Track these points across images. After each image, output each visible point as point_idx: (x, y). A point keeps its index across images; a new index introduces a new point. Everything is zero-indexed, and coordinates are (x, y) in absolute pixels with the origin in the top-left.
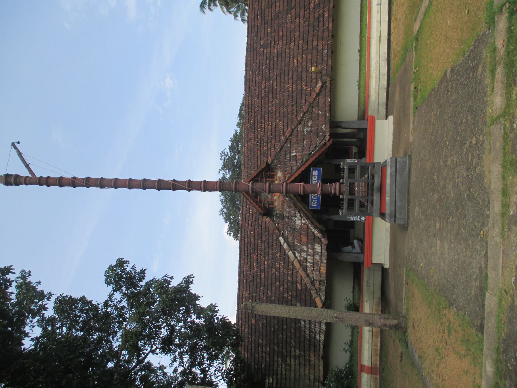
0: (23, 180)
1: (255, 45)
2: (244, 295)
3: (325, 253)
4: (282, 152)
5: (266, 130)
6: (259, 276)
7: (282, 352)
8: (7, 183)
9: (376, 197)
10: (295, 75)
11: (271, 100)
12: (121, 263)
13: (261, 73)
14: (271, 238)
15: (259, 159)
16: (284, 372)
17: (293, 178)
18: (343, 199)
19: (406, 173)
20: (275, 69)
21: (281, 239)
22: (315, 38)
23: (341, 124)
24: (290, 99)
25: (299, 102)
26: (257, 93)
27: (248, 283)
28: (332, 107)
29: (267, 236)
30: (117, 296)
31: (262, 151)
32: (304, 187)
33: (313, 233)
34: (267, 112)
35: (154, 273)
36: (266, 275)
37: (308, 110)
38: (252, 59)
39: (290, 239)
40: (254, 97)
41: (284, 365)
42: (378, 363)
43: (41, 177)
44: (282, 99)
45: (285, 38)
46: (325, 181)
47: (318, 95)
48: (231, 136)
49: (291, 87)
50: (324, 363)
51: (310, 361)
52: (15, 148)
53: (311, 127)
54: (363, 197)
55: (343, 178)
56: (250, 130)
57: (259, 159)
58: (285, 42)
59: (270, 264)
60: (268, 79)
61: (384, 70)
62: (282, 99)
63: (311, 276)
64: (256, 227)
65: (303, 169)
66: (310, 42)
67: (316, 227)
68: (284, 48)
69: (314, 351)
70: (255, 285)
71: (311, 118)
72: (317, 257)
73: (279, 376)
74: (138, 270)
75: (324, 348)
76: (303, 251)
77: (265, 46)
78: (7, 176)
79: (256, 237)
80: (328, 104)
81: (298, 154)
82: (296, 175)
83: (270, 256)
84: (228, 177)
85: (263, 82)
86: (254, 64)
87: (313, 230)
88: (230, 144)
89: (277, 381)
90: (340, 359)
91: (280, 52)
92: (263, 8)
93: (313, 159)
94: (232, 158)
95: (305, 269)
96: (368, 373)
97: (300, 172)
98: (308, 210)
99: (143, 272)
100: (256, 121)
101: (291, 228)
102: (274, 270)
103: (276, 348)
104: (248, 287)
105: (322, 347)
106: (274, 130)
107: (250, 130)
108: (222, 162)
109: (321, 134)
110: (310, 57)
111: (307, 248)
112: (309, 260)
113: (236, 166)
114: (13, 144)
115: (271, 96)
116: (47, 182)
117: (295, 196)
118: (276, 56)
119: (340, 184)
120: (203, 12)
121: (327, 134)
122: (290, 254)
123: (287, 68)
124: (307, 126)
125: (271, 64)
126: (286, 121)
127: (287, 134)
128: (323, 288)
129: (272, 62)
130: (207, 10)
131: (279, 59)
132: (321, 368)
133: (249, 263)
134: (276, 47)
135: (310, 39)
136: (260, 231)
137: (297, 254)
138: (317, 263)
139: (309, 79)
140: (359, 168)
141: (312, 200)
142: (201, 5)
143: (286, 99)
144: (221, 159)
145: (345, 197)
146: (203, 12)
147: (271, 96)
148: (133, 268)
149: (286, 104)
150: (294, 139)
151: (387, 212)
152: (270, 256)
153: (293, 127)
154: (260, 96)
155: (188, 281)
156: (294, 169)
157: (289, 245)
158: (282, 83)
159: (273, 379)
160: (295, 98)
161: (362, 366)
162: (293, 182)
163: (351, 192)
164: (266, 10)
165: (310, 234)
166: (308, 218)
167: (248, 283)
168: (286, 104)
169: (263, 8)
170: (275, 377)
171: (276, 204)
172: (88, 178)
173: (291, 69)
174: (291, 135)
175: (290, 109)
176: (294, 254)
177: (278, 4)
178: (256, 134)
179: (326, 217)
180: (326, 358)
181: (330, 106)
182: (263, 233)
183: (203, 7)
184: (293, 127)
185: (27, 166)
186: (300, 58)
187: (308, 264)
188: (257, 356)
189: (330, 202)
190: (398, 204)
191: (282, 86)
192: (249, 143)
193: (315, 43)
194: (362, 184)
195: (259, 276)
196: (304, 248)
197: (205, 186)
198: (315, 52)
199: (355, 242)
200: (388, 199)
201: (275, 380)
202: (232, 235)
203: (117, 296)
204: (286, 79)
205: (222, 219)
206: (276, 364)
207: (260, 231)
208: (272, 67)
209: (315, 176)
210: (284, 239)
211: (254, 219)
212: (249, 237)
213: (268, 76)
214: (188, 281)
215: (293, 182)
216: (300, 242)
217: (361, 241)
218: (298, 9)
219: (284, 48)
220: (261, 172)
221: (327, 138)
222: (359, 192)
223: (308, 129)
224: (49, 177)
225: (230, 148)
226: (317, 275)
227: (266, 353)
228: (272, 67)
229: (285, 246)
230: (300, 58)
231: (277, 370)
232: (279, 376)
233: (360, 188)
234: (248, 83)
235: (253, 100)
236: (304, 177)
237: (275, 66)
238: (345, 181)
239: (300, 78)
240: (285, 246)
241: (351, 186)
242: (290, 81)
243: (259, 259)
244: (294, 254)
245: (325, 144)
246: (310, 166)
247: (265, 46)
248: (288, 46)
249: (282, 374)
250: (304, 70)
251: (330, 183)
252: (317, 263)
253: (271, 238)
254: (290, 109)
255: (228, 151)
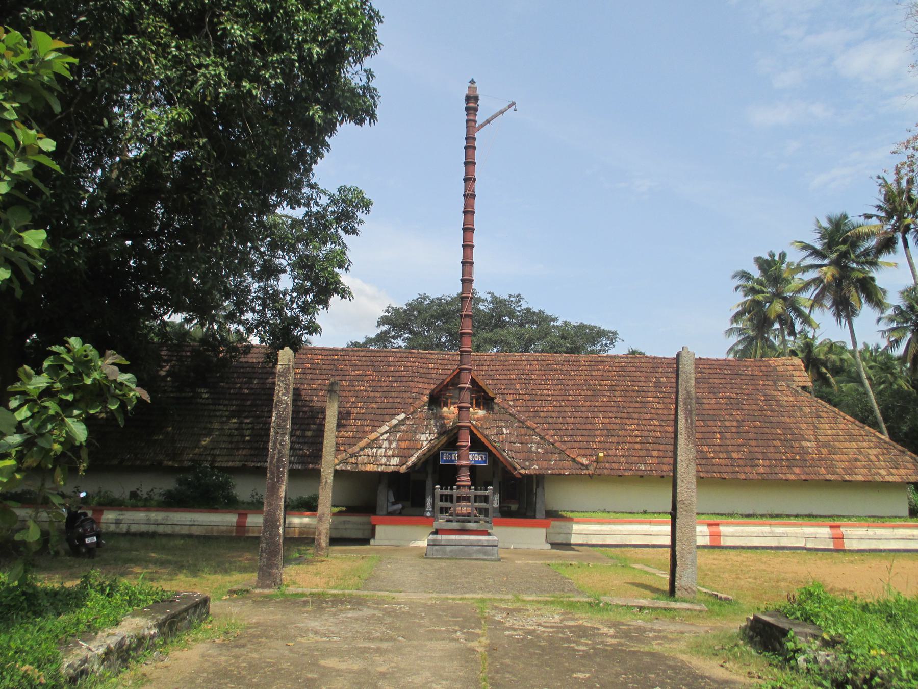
0: (471, 118)
1: (660, 370)
2: (315, 357)
3: (390, 469)
4: (507, 416)
5: (542, 387)
6: (344, 378)
7: (245, 411)
8: (468, 99)
9: (455, 525)
10: (615, 427)
11: (583, 393)
12: (366, 205)
13: (622, 378)
14: (396, 395)
15: (504, 377)
16: (218, 414)
17: (475, 432)
18: (452, 489)
19: (481, 556)
20: (625, 399)
21: (403, 416)
22: (661, 454)
23: (540, 488)
24: (582, 421)
25: (579, 432)
26: (594, 373)
27: (333, 363)
28: (594, 478)
29: (399, 389)
30: (324, 200)
31: (513, 382)
32: (465, 446)
33: (412, 456)
34: (568, 388)
35: (354, 246)
36: (346, 389)
37: (556, 448)
38: (642, 365)
39: (403, 427)
40: (588, 368)
41: (227, 413)
42: (251, 535)
43: (475, 139)
44: (584, 409)
45: (665, 412)
46: (473, 469)
47: (574, 460)
48: (548, 312)
49: (600, 421)
50: (237, 468)
51: (238, 449)
52: (509, 107)
53: (537, 452)
54: (455, 510)
55: (476, 489)
56: (544, 363)
57: (504, 377)
58: (660, 412)
59: (360, 394)
60: (612, 389)
61: (609, 541)
62: (584, 409)
63: (362, 453)
64: (411, 374)
65: (487, 443)
66: (656, 446)
67: (419, 459)
68: (653, 411)
69: (251, 455)
70: (330, 372)
71: (546, 452)
72: (384, 460)
73: (211, 407)
74: (359, 228)
75: (257, 467)
76: (390, 444)
77: (658, 384)
78: (476, 99)
79: (398, 374)
80: (562, 472)
81: (504, 437)
82: (479, 436)
83: (372, 394)
84: (481, 307)
85: (609, 383)
86: (634, 369)
87: (416, 456)
88: (535, 310)
89: (204, 404)
90: (243, 489)
91: (647, 405)
92: (711, 381)
93: (498, 456)
94: (512, 314)
95: (369, 446)
96: (237, 522)
97: (483, 440)
98: (439, 450)
99: (354, 232)
100: (556, 372)
101: (416, 428)
102: (353, 399)
103: (249, 403)
104: (328, 362)
105: (259, 465)
106: (543, 398)
107: (544, 363)
108: (506, 297)
109: (527, 464)
110: (638, 446)
111: (394, 449)
112: (380, 451)
113: (500, 320)
114: (514, 103)
115: (589, 393)
116: (470, 147)
117: (455, 434)
118: (643, 400)
119: (469, 487)
120: (735, 276)
121: (527, 471)
122: (385, 428)
123: (625, 416)
124: (538, 448)
125: (632, 394)
126: (554, 415)
127: (529, 423)
128: (349, 468)
129: (635, 394)
130: (737, 282)
131: (637, 405)
132: (230, 464)
133: (360, 363)
134: (655, 400)
135: (661, 447)
136: (405, 379)
137: (385, 436)
138: (377, 461)
139: (607, 445)
140: (487, 506)
141: (451, 454)
142: (745, 272)
143: (584, 415)
144: (510, 296)
145: (455, 492)
146: (735, 276)
147: (589, 393)
148: (361, 222)
149: (576, 415)
150: (522, 431)
151: (439, 537)
152: (372, 394)
153: (537, 430)
154: (589, 378)
155: (345, 293)
156: (487, 432)
157: (396, 426)
158: (606, 409)
159: (207, 398)
160: (584, 427)
161: (245, 515)
162: (472, 433)
163: (460, 499)
164: (706, 386)
165: (411, 452)
166: (429, 450)
167: (333, 363)
168: (576, 415)
169: (711, 381)
170: (210, 401)
171: (445, 409)
172: (474, 196)
173: (624, 421)
174: (528, 427)
175: (569, 420)
176: (386, 433)
177: (713, 401)
178: (538, 372)
179: (430, 470)
180: (243, 471)
181: (560, 474)
182: (402, 384)
183: (742, 276)
184: (537, 430)
185: (488, 122)
186: (637, 433)
187: (375, 450)
188: (235, 375)
189: (448, 475)
190: (448, 548)
191: (601, 409)
192: (525, 363)
193: (655, 453)
194: (469, 510)
195: (344, 378)
196: (394, 445)
197: (466, 281)
198: (643, 453)
199: (399, 506)
200: (453, 537)
201: (207, 402)
202: (387, 314)
203: (324, 200)
204: (611, 414)
205: (413, 296)
206: (227, 402)
207: (405, 379)
208: (628, 394)
209: (476, 458)
210: (403, 420)
211: (422, 371)
212: (396, 364)
213: (617, 388)
214: (345, 293)
215: (472, 433)
216: (401, 440)
217: (400, 514)
218: (703, 429)
219: (653, 411)
220: (484, 391)
221: (523, 471)
222: (460, 506)
223: (534, 449)
224: (475, 148)
225: (528, 310)
226: (363, 460)
227: (240, 388)
228: (628, 394)
229: (394, 421)
230: (637, 433)
231: (220, 404)
232: (211, 407)
233: (464, 508)
234: (609, 360)
235: (584, 368)
236: (477, 445)
237: (629, 399)
238: (472, 492)
239: (610, 433)
240: (394, 421)
241: (466, 499)
242: (608, 420)
243: (367, 378)
244: (386, 433)
245: (515, 469)
246: (490, 452)
247: (658, 384)
248: (655, 416)
249: (215, 410)
250: (621, 439)
251: (470, 475)
252: (377, 461)
253: (396, 395)
254: (569, 420)
255: (523, 307)
